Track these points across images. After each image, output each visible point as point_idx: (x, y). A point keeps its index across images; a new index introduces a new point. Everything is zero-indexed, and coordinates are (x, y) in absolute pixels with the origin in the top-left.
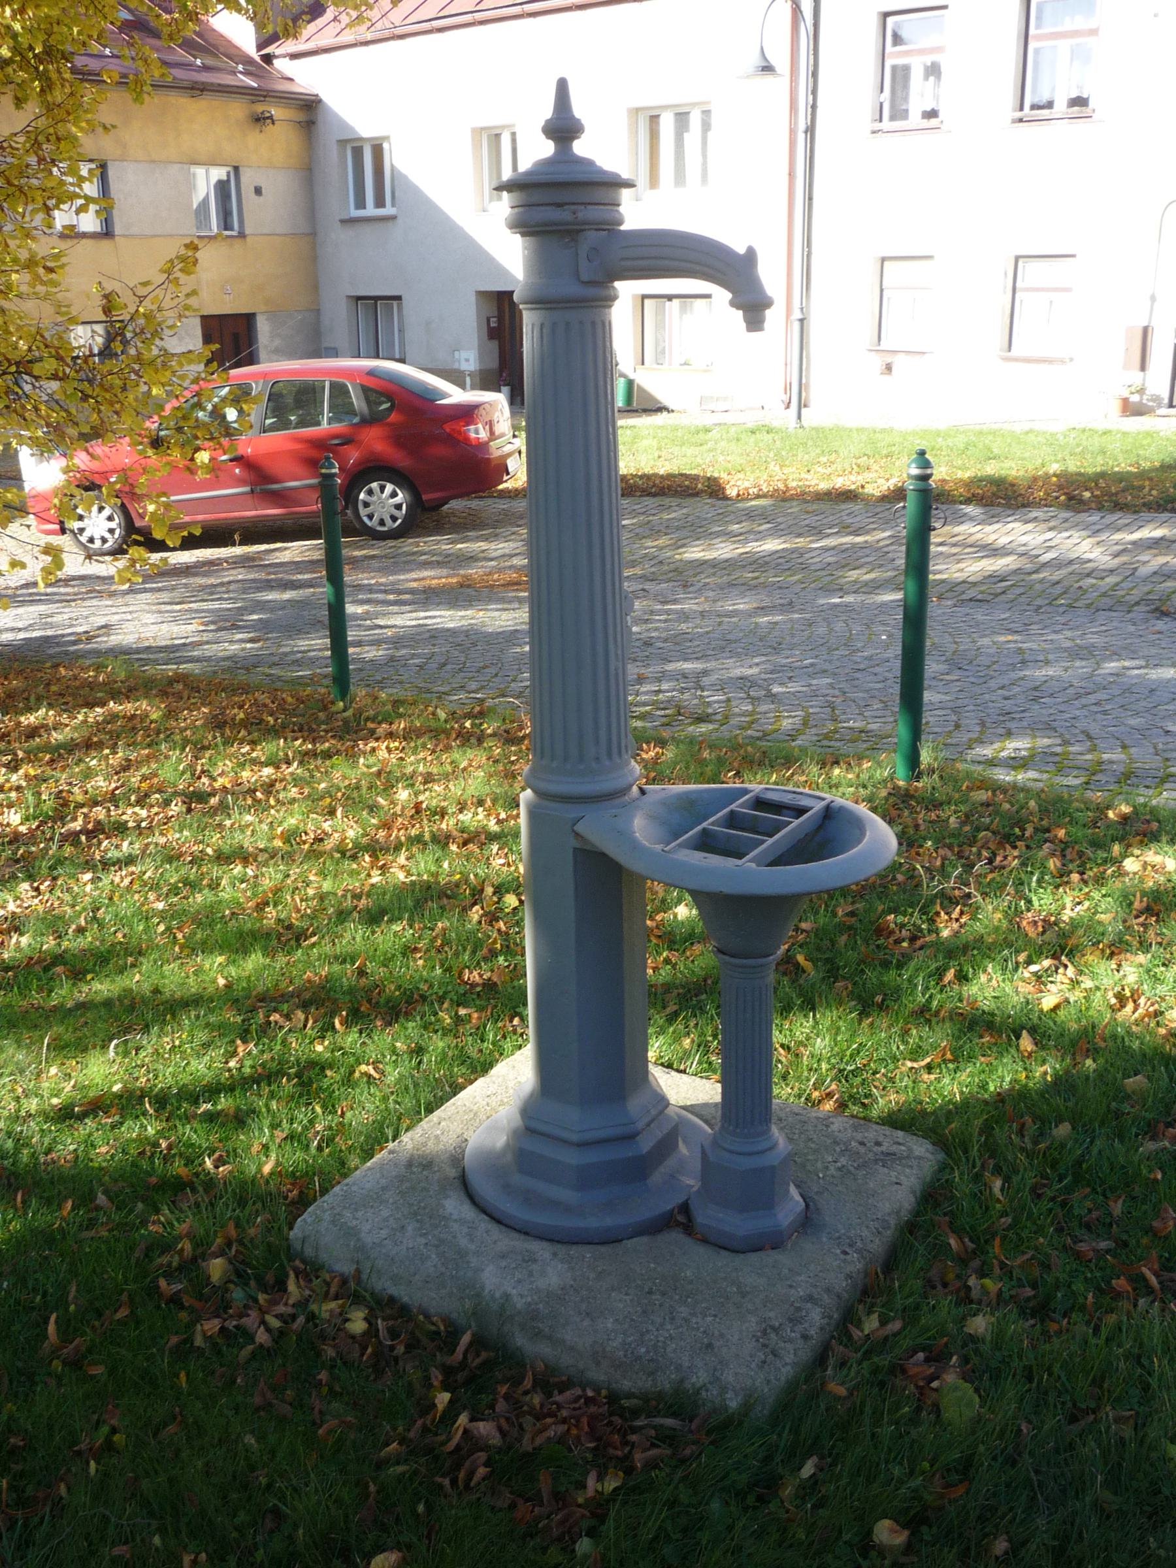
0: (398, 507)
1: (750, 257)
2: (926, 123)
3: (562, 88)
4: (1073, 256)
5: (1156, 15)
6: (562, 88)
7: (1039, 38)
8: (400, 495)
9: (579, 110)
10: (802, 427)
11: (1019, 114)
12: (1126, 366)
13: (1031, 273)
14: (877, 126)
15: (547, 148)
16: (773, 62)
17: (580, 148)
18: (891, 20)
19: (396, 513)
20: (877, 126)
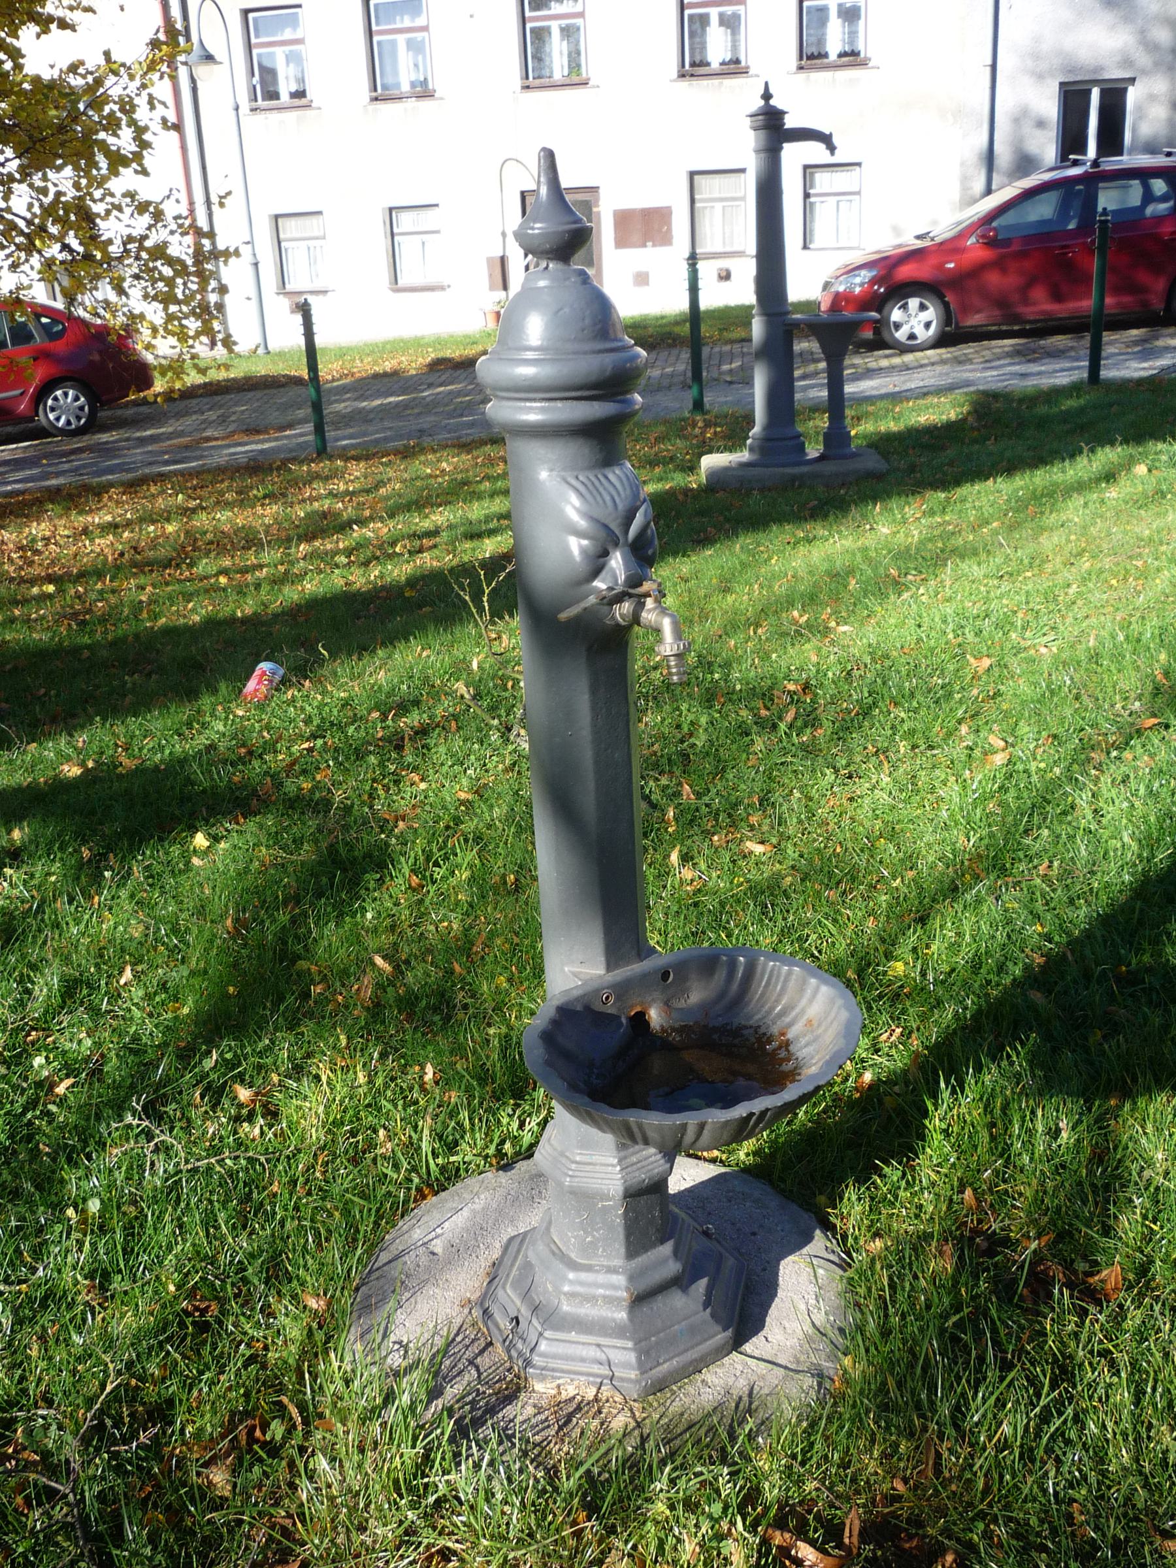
0: (81, 408)
1: (831, 134)
2: (297, 102)
3: (766, 84)
4: (437, 205)
5: (471, 16)
6: (766, 84)
7: (381, 33)
8: (82, 399)
9: (771, 91)
10: (269, 353)
11: (374, 94)
12: (492, 288)
13: (405, 221)
14: (254, 104)
15: (762, 103)
16: (212, 51)
17: (772, 102)
18: (251, 16)
19: (80, 413)
20: (254, 104)
